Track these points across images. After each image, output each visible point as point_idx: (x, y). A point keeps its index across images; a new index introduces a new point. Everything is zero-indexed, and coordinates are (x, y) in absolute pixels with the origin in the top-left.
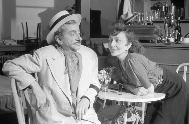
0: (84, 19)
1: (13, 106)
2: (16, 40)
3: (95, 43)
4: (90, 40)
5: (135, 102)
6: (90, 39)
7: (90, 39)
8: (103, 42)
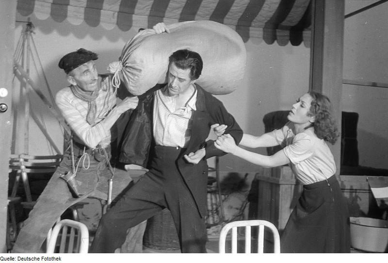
3: (351, 187)
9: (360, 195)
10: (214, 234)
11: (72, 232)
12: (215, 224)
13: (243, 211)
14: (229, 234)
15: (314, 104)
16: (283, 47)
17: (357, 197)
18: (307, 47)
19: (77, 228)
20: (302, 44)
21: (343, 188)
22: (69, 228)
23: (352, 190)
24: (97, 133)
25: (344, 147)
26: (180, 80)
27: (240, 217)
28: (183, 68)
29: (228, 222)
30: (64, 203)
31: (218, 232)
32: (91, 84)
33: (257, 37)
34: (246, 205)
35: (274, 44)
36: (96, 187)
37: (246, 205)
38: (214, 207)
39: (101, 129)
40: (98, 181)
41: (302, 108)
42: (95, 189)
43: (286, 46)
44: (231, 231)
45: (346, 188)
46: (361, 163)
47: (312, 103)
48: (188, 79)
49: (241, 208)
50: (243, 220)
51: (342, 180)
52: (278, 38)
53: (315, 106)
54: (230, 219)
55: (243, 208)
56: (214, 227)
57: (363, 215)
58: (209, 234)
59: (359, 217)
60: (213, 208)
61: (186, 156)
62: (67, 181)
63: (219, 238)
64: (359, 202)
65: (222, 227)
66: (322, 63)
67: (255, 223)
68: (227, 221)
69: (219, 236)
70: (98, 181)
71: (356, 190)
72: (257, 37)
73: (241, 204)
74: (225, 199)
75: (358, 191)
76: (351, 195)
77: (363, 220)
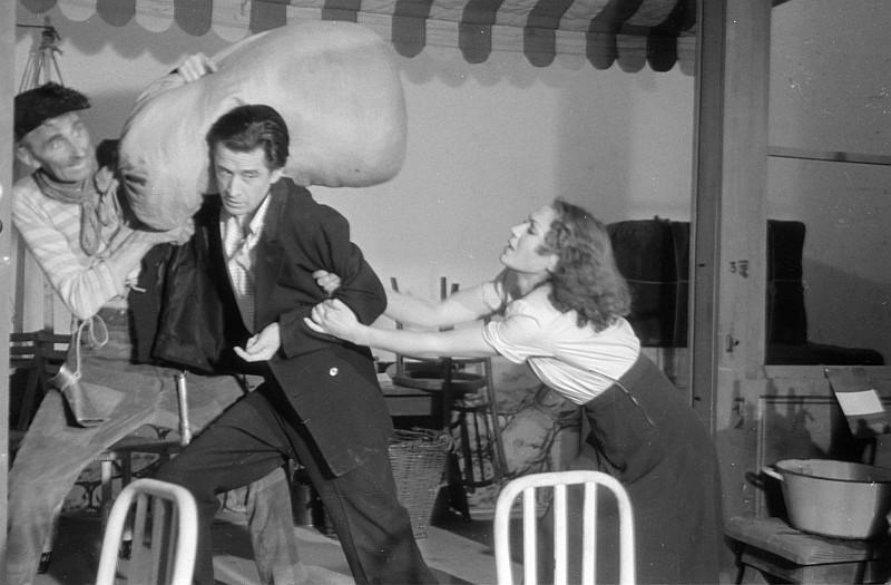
0: (739, 269)
1: (75, 421)
2: (84, 180)
3: (792, 390)
4: (765, 376)
5: (561, 470)
6: (764, 370)
7: (764, 370)
8: (833, 382)
9: (811, 409)
10: (483, 505)
11: (159, 511)
12: (484, 483)
13: (548, 451)
14: (518, 504)
15: (558, 226)
16: (632, 74)
17: (804, 413)
18: (688, 74)
19: (168, 497)
20: (677, 65)
21: (772, 394)
22: (150, 499)
23: (793, 399)
24: (97, 285)
25: (773, 300)
26: (248, 174)
27: (543, 464)
28: (246, 149)
29: (513, 476)
30: (85, 445)
31: (493, 500)
32: (71, 166)
33: (574, 54)
34: (554, 436)
35: (612, 67)
36: (159, 401)
37: (554, 436)
38: (484, 443)
39: (107, 277)
40: (161, 389)
41: (530, 236)
42: (156, 405)
43: (640, 73)
44: (521, 496)
45: (780, 393)
46: (812, 337)
47: (554, 225)
48: (264, 170)
49: (544, 444)
50: (549, 470)
51: (771, 375)
52: (621, 54)
53: (559, 231)
54: (518, 471)
55: (548, 444)
56: (483, 489)
57: (818, 453)
58: (473, 506)
59: (809, 459)
60: (479, 446)
61: (238, 350)
62: (63, 389)
63: (494, 514)
64: (809, 425)
65: (501, 489)
66: (721, 106)
67: (575, 477)
68: (514, 472)
69: (495, 508)
70: (161, 389)
71: (802, 397)
72: (574, 54)
73: (544, 435)
74: (507, 425)
75: (806, 400)
76: (791, 410)
77: (816, 466)
